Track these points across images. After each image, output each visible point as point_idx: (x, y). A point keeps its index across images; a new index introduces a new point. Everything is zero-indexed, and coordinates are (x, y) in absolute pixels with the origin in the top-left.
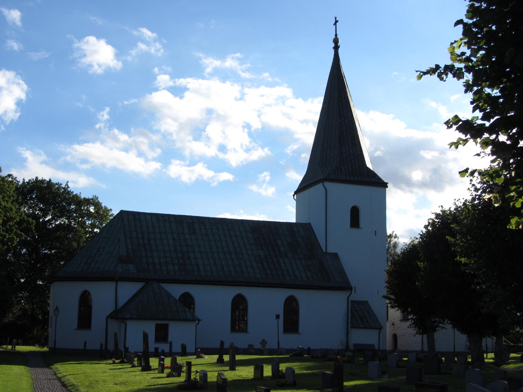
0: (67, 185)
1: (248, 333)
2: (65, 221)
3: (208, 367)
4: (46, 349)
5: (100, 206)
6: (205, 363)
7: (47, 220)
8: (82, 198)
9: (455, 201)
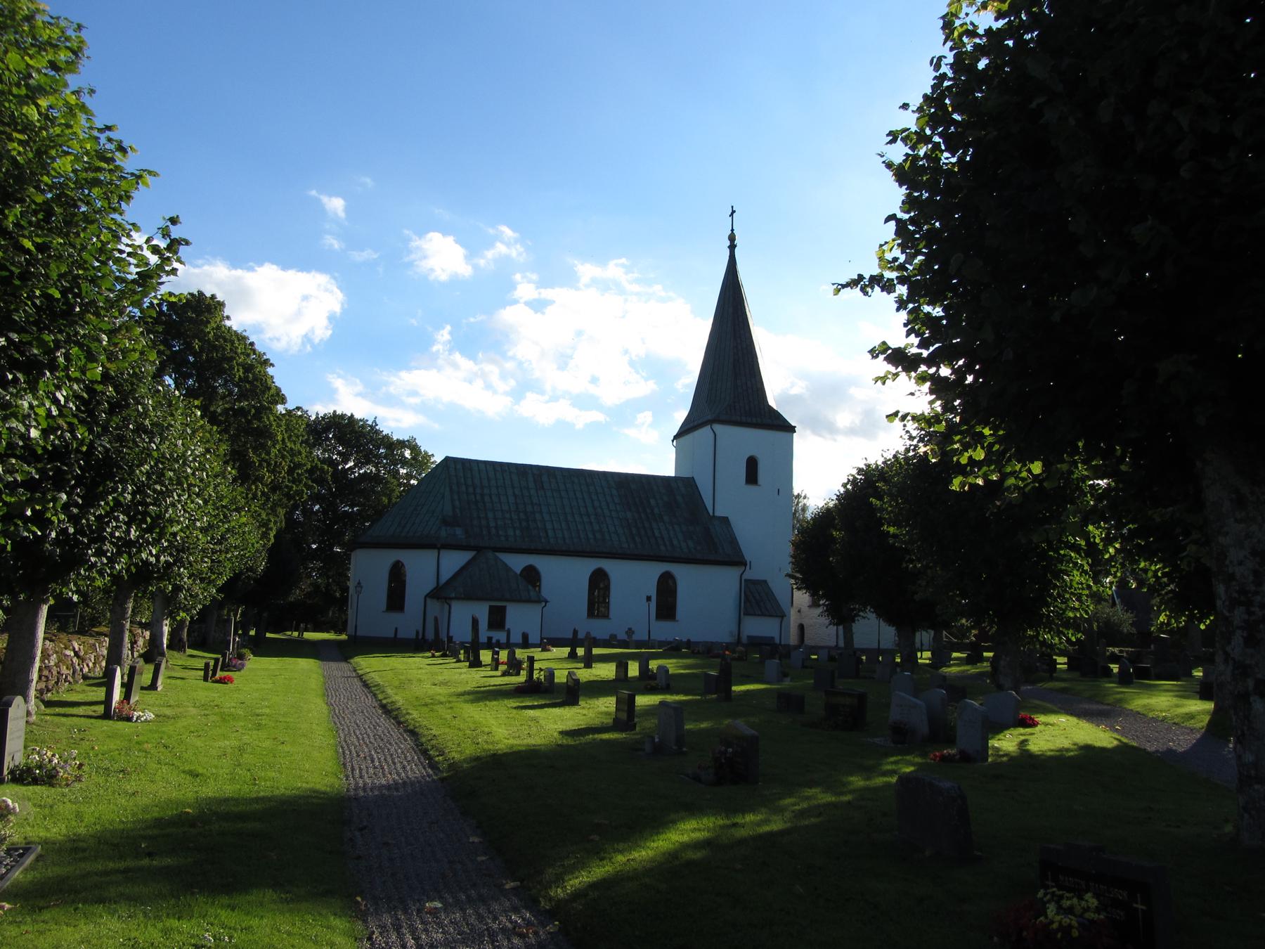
1: (610, 619)
4: (344, 637)
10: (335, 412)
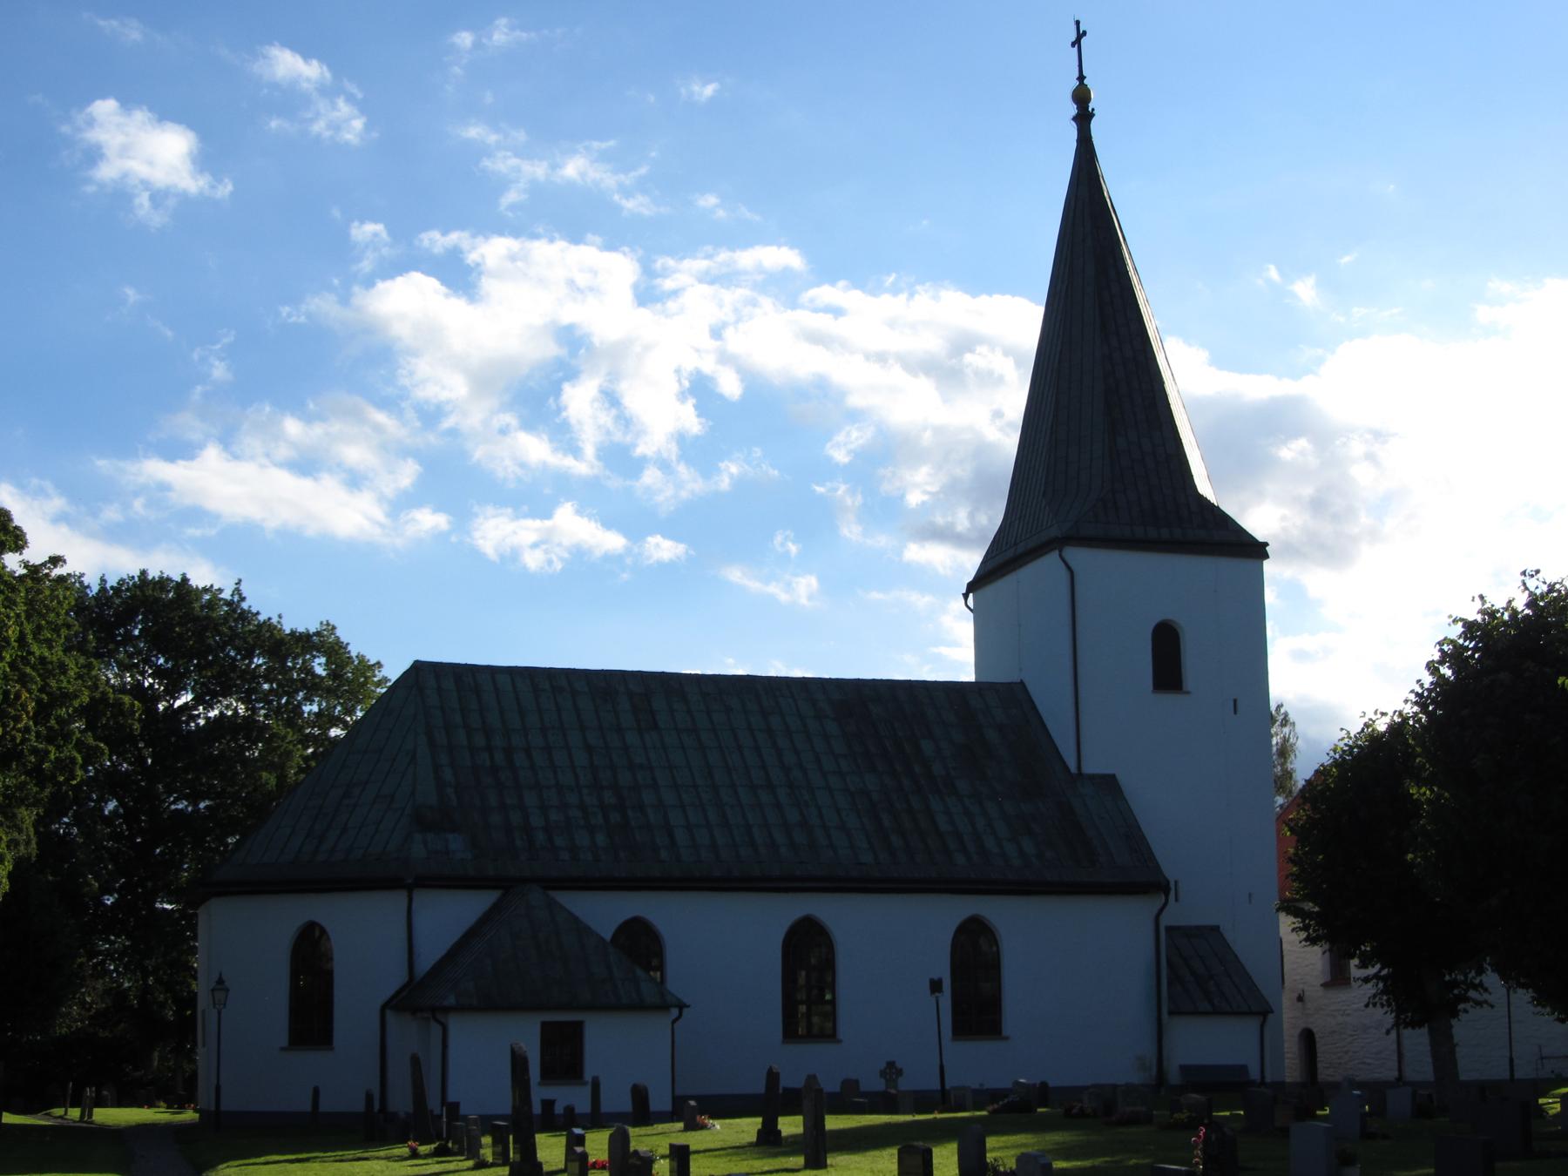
0: (237, 591)
1: (839, 1041)
2: (237, 706)
3: (730, 1161)
4: (189, 1116)
5: (345, 653)
6: (719, 1147)
7: (179, 707)
8: (288, 632)
9: (1523, 577)
10: (143, 573)
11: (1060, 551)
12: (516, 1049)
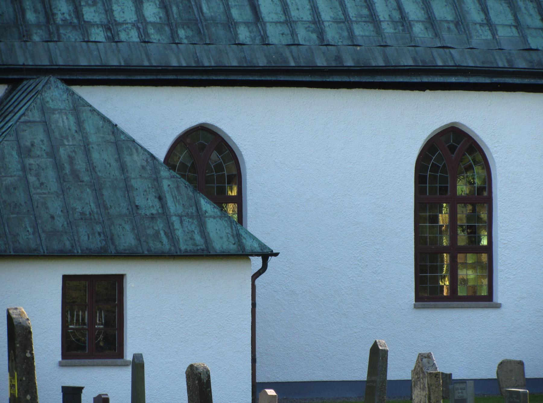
1: (498, 306)
11: (422, 22)
12: (14, 316)
